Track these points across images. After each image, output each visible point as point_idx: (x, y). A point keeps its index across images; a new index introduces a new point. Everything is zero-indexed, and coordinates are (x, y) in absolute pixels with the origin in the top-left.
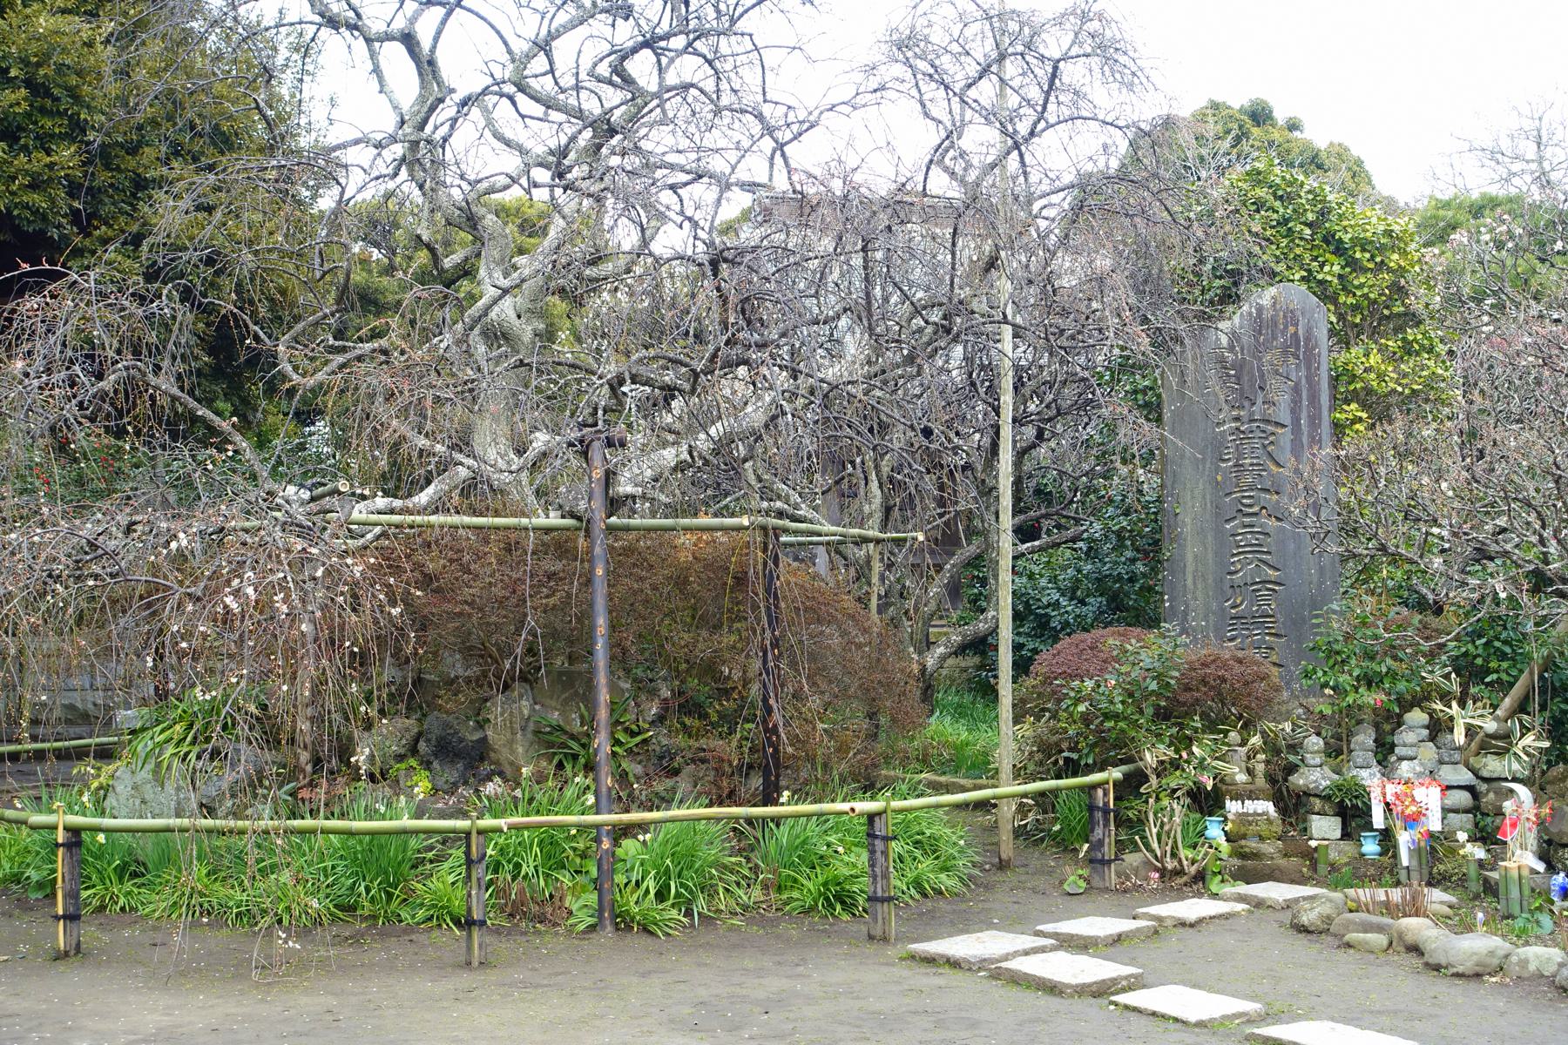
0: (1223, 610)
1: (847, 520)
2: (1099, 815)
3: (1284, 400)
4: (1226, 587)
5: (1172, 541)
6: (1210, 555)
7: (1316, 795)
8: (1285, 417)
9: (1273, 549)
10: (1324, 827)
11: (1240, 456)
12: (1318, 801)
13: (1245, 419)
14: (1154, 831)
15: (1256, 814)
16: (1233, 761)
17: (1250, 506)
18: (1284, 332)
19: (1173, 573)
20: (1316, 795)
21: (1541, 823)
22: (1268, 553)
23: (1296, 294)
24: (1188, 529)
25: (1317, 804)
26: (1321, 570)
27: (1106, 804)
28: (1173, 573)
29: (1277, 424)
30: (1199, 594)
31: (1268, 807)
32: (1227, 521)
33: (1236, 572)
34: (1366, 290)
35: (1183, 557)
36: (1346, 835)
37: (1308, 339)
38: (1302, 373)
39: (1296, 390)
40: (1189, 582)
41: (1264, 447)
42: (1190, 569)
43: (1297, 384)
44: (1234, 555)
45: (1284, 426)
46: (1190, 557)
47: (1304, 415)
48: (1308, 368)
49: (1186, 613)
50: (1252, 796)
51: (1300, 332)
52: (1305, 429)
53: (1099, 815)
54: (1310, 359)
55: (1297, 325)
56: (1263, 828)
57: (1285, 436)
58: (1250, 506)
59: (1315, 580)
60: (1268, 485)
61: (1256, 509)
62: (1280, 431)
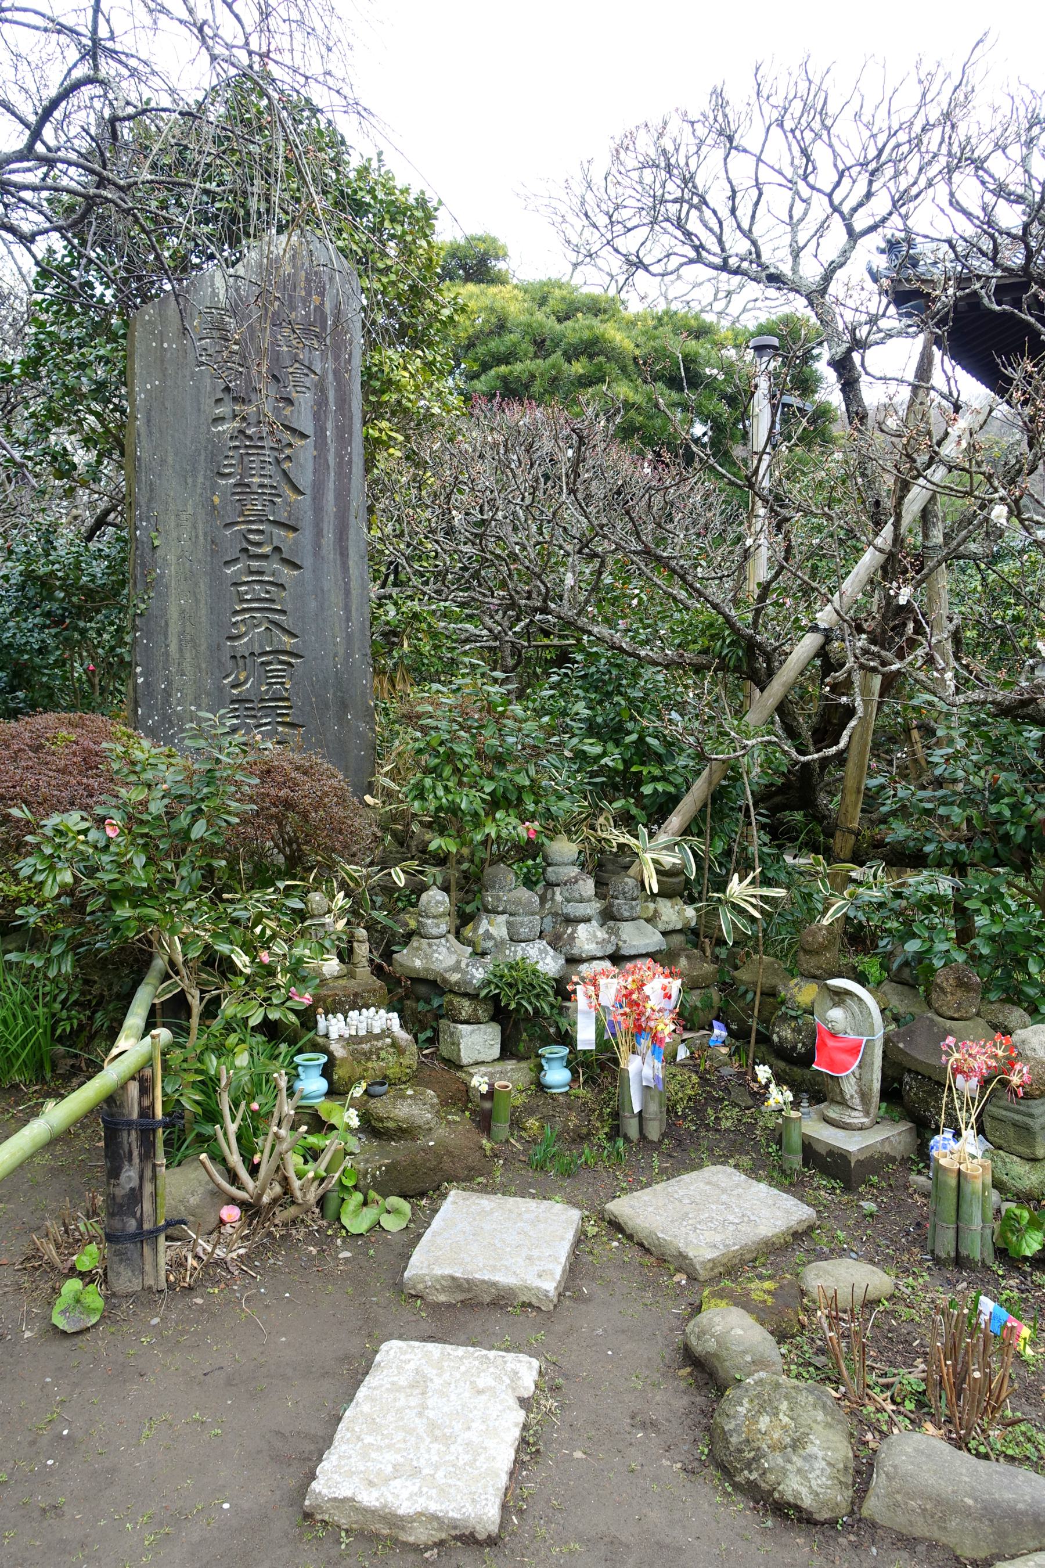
0: (221, 689)
1: (592, 1231)
2: (131, 1139)
3: (305, 400)
4: (226, 658)
5: (148, 586)
6: (203, 612)
7: (466, 995)
8: (306, 425)
9: (289, 607)
10: (477, 1042)
11: (246, 472)
12: (466, 1003)
13: (253, 420)
14: (233, 1128)
15: (371, 1036)
16: (317, 938)
17: (259, 544)
18: (305, 302)
19: (149, 634)
20: (466, 995)
21: (887, 1040)
22: (283, 612)
23: (326, 251)
24: (171, 571)
25: (466, 1008)
26: (349, 638)
27: (146, 1112)
28: (149, 634)
29: (293, 431)
30: (187, 666)
31: (381, 1020)
32: (227, 563)
33: (239, 637)
34: (393, 277)
35: (165, 610)
36: (507, 1051)
37: (337, 322)
38: (330, 365)
39: (321, 388)
40: (173, 648)
41: (278, 462)
42: (174, 629)
43: (322, 378)
44: (236, 613)
45: (304, 436)
46: (173, 613)
47: (330, 425)
48: (337, 358)
49: (167, 693)
50: (357, 1002)
51: (328, 308)
52: (332, 447)
53: (131, 1139)
54: (339, 347)
55: (322, 294)
56: (389, 1064)
57: (305, 450)
58: (259, 544)
59: (341, 652)
60: (283, 517)
61: (266, 549)
62: (299, 442)
